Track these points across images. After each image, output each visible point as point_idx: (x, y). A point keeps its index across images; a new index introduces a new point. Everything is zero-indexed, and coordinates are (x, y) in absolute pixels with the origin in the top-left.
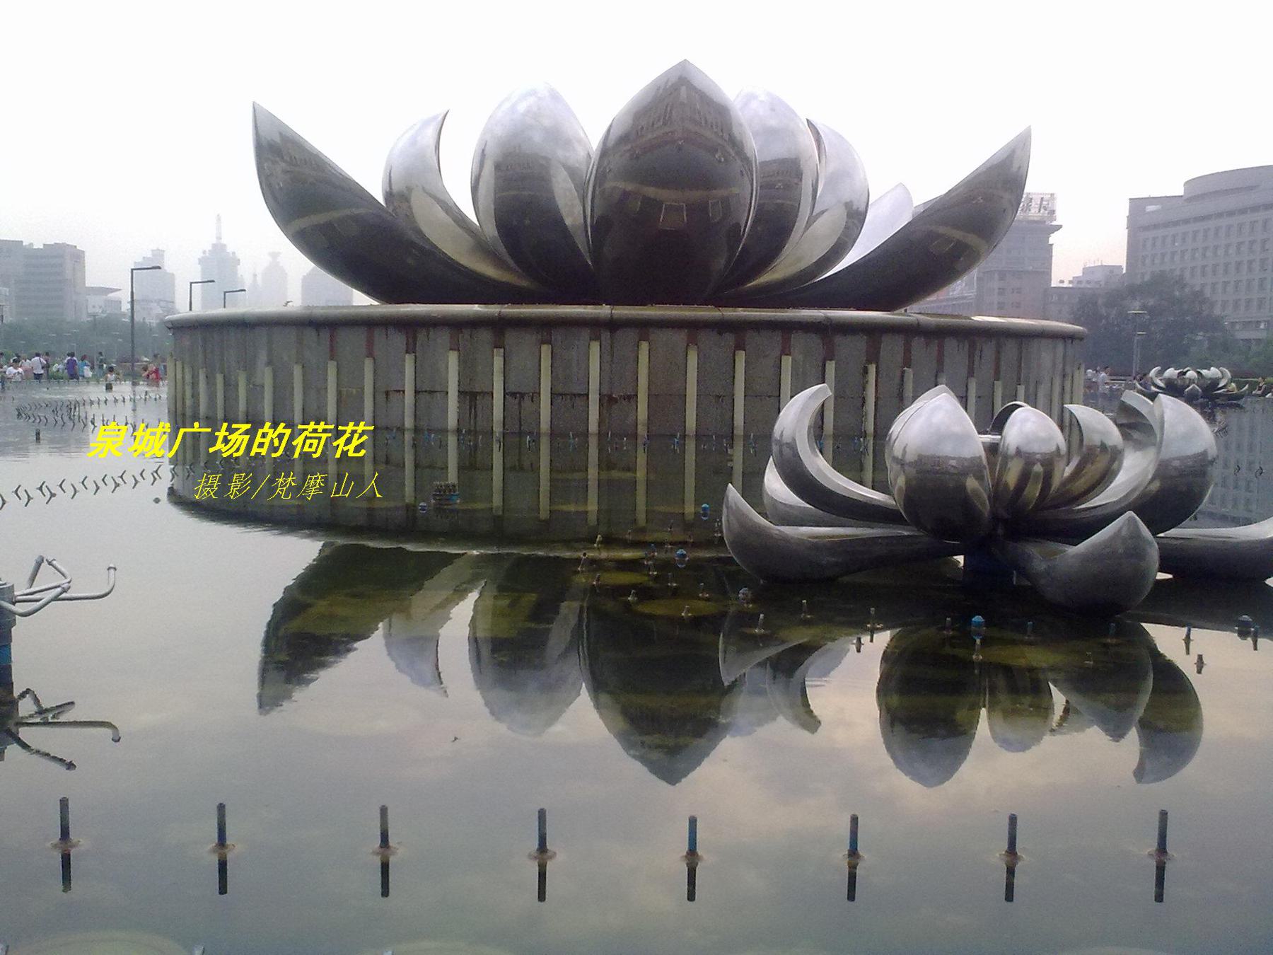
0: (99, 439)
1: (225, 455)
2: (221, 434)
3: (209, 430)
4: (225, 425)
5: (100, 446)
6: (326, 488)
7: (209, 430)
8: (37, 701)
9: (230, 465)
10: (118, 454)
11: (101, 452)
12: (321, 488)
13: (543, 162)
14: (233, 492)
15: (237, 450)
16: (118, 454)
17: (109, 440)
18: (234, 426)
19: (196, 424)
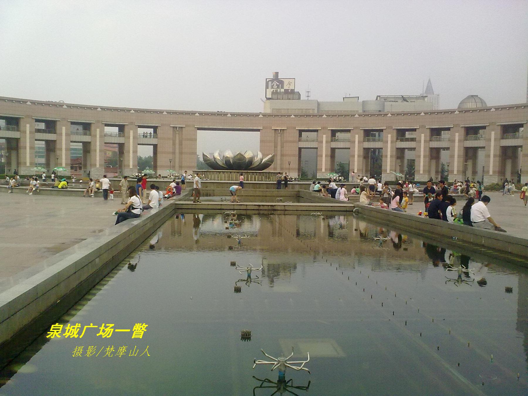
0: (51, 330)
1: (103, 337)
2: (102, 328)
3: (97, 327)
4: (103, 325)
5: (52, 333)
6: (127, 353)
7: (97, 327)
8: (292, 383)
9: (107, 342)
10: (59, 337)
11: (52, 336)
12: (125, 352)
13: (239, 157)
14: (88, 354)
15: (109, 335)
16: (59, 337)
17: (55, 331)
18: (107, 325)
19: (92, 324)
